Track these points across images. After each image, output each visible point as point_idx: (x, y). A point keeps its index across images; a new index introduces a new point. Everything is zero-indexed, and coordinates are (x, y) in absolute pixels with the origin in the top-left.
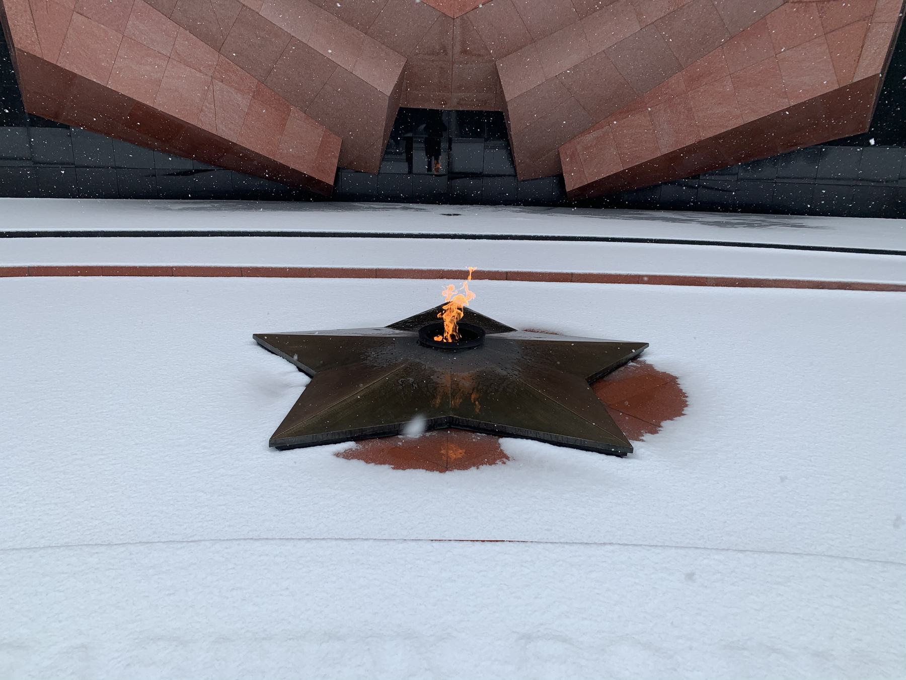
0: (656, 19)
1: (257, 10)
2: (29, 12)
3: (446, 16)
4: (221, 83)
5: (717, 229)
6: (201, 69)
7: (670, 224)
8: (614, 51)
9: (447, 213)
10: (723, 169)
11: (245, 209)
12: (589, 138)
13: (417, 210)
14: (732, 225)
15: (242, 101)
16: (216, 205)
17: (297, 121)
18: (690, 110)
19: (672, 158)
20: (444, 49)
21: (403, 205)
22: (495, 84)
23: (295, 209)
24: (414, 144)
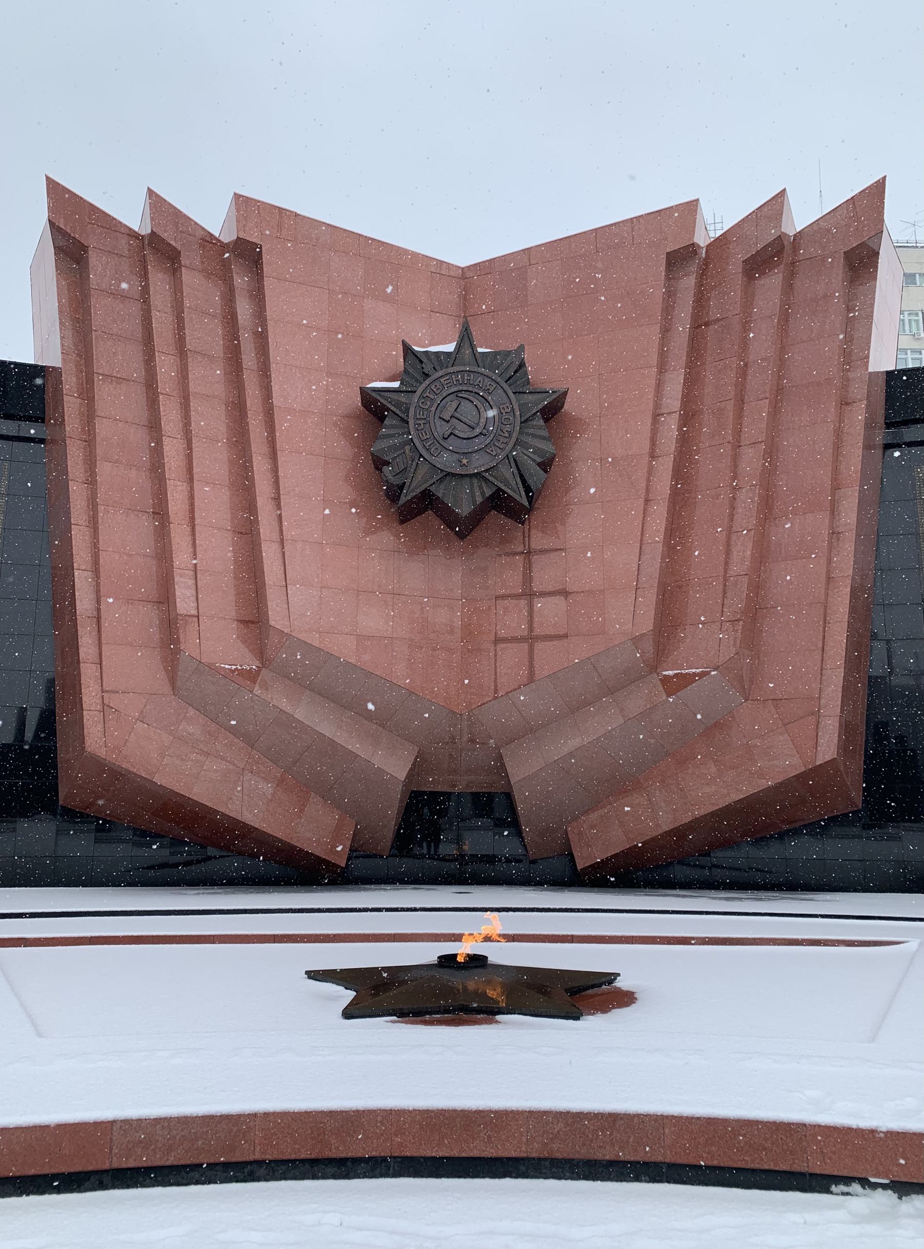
0: (636, 714)
1: (292, 714)
2: (102, 722)
3: (454, 713)
4: (250, 774)
5: (724, 902)
6: (235, 762)
7: (680, 899)
8: (676, 660)
9: (902, 945)
10: (727, 844)
11: (257, 893)
12: (594, 816)
13: (428, 889)
14: (740, 899)
15: (267, 788)
16: (228, 890)
17: (316, 808)
18: (682, 790)
19: (679, 833)
20: (453, 738)
21: (413, 886)
22: (501, 769)
23: (245, 892)
24: (402, 775)
